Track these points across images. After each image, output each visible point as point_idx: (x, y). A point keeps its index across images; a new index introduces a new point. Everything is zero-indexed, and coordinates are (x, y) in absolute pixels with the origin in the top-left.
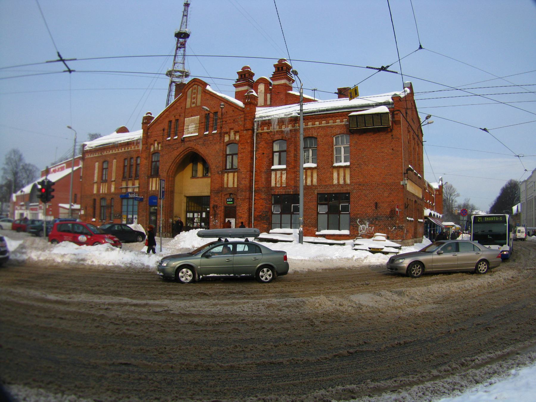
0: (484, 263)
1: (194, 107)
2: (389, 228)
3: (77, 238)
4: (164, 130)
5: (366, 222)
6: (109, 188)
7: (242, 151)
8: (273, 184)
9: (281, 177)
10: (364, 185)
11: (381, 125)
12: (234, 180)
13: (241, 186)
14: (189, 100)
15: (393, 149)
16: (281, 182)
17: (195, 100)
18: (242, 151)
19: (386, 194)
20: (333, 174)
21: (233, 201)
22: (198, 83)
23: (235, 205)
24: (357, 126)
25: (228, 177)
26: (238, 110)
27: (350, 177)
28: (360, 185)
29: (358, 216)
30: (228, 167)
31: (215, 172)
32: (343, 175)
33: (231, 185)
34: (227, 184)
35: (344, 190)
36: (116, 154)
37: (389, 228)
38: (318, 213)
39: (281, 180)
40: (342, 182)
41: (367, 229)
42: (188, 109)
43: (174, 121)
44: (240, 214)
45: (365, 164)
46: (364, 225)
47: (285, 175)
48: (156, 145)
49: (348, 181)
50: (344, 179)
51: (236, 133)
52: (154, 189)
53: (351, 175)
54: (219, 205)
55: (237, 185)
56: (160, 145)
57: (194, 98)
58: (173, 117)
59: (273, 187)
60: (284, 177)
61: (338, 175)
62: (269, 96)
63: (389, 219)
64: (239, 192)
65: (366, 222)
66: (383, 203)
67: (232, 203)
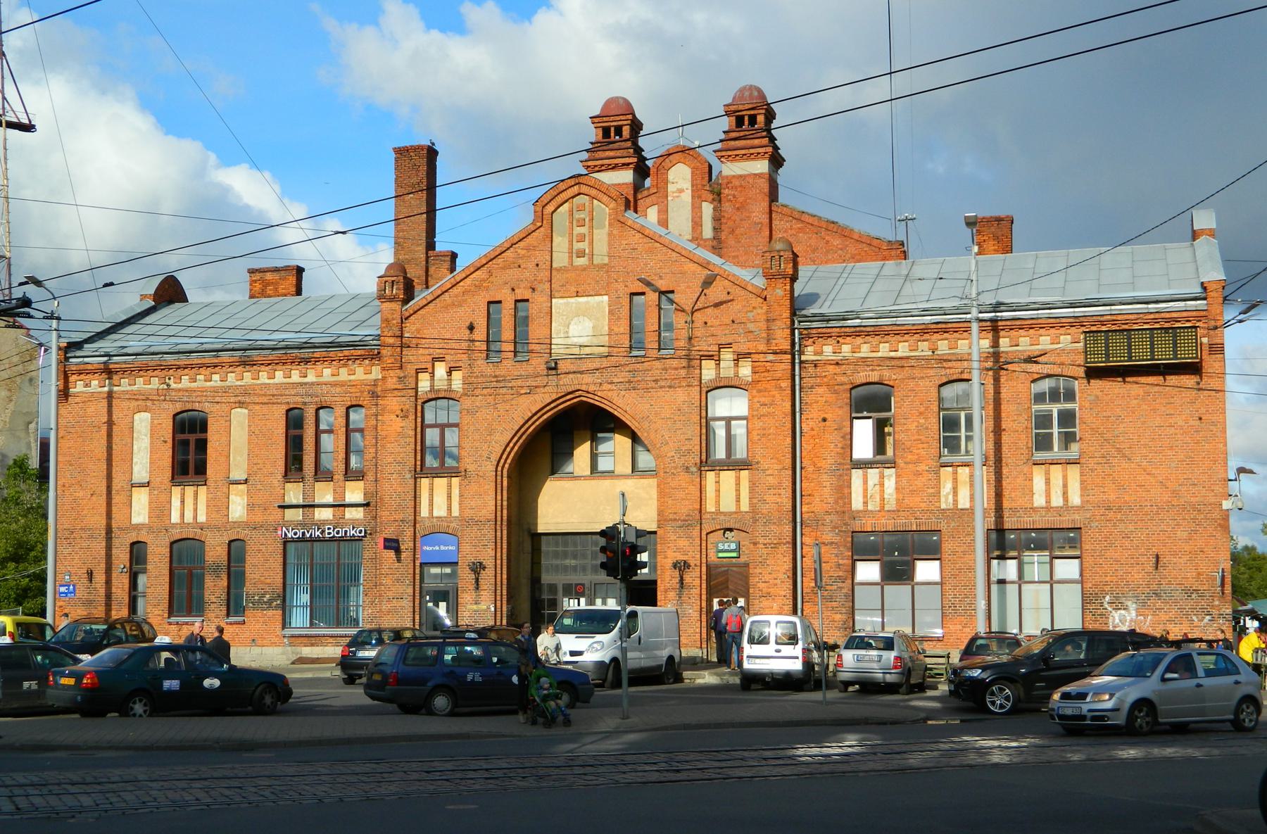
0: (1145, 709)
1: (584, 269)
2: (1194, 618)
3: (383, 678)
4: (471, 328)
5: (1129, 603)
6: (219, 506)
7: (764, 410)
8: (857, 503)
9: (882, 485)
10: (1120, 509)
11: (1130, 359)
12: (738, 490)
13: (764, 509)
14: (560, 242)
15: (1200, 419)
16: (883, 499)
17: (584, 246)
18: (764, 410)
19: (1182, 534)
20: (1031, 480)
21: (738, 549)
22: (594, 192)
23: (743, 559)
24: (1107, 355)
25: (718, 482)
26: (743, 292)
27: (1082, 489)
28: (1109, 509)
29: (1107, 588)
30: (720, 453)
31: (676, 468)
32: (1061, 483)
33: (728, 505)
34: (718, 503)
35: (196, 533)
36: (246, 391)
37: (1194, 618)
38: (1082, 582)
39: (882, 491)
40: (1057, 501)
41: (1131, 620)
42: (559, 270)
43: (508, 306)
44: (761, 585)
45: (1124, 456)
46: (1123, 612)
47: (893, 480)
48: (441, 370)
49: (1075, 499)
50: (1065, 494)
51: (739, 357)
52: (440, 511)
53: (1082, 482)
54: (692, 563)
55: (751, 504)
56: (457, 375)
57: (581, 238)
58: (506, 291)
59: (858, 512)
60: (890, 485)
61: (1048, 482)
62: (707, 209)
63: (1193, 596)
64: (760, 523)
65: (1129, 603)
66: (1175, 554)
67: (734, 555)
